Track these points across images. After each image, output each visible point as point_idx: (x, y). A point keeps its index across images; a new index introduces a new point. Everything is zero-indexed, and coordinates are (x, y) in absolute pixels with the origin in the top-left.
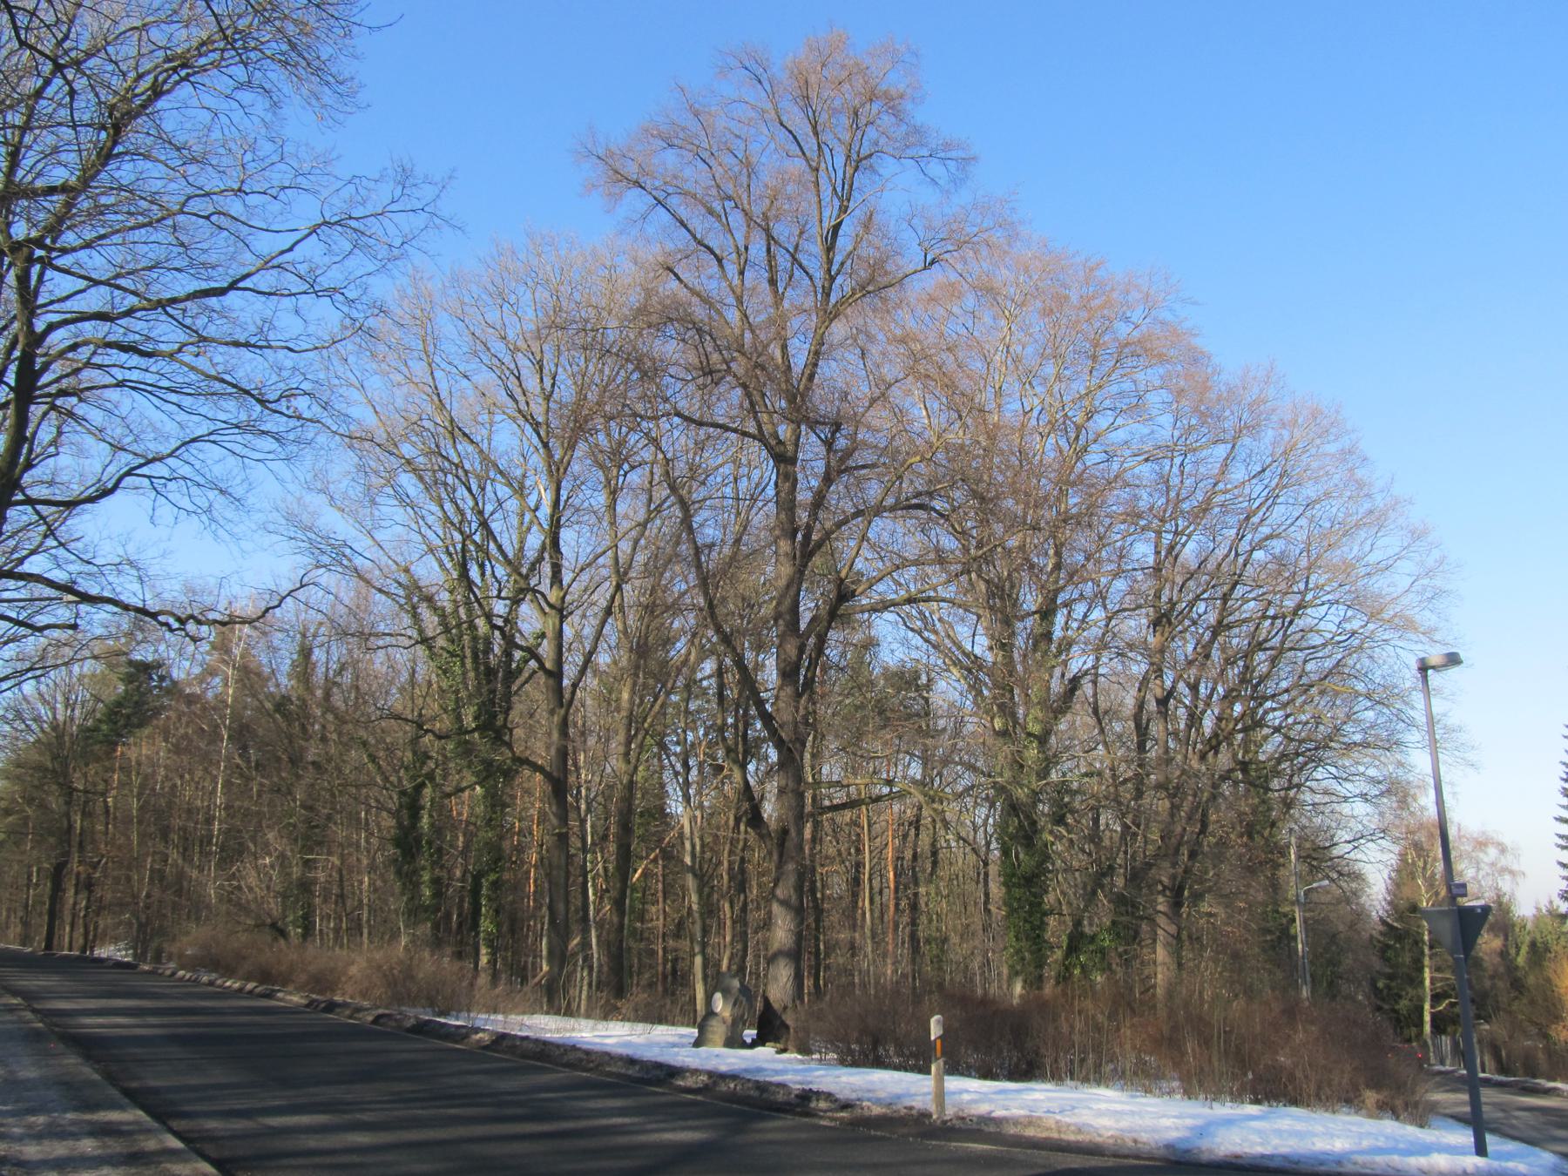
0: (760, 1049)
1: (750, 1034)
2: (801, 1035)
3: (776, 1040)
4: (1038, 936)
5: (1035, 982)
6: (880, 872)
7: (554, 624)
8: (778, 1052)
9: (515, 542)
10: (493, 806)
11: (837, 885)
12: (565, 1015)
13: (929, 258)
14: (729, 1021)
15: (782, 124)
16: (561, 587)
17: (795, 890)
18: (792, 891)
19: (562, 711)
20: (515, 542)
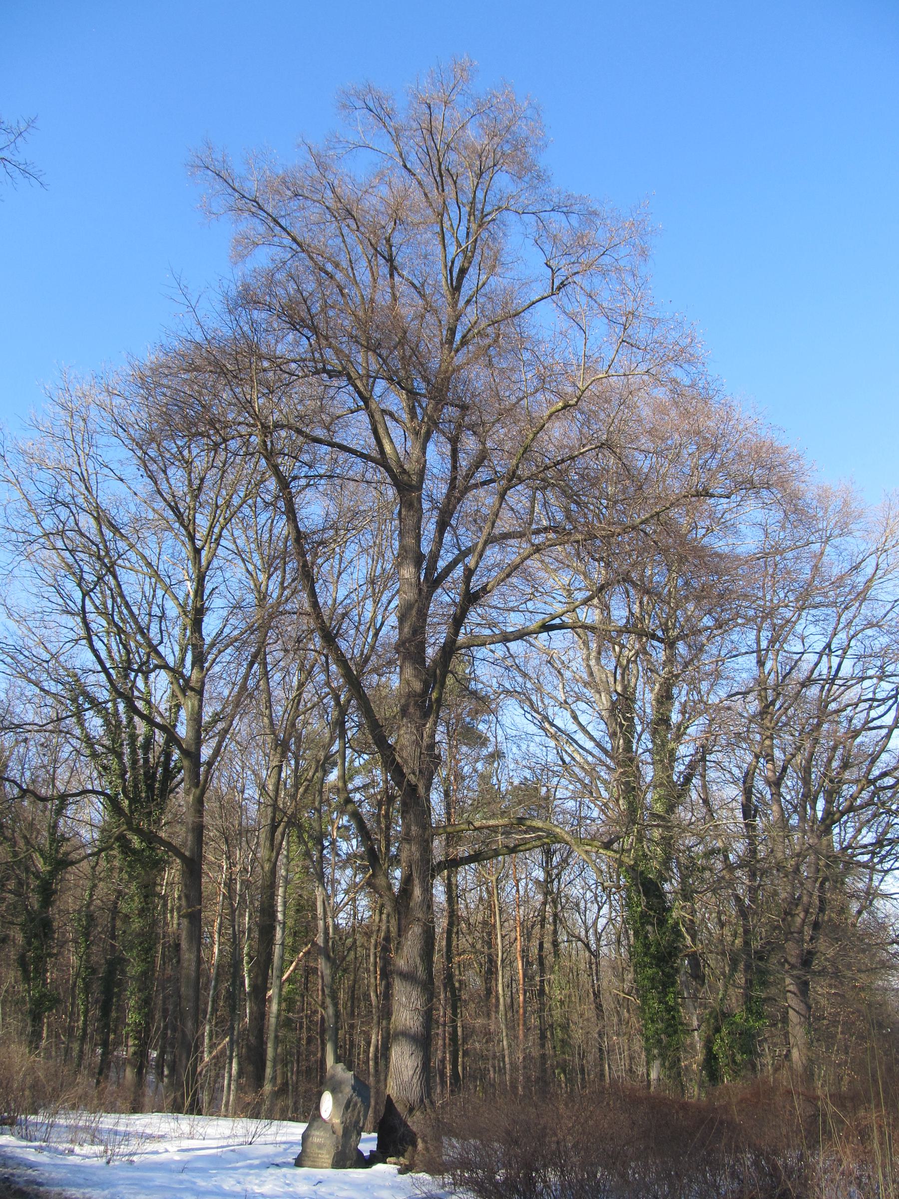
0: (379, 1167)
1: (368, 1143)
2: (493, 969)
3: (399, 1153)
4: (673, 1017)
5: (674, 1068)
6: (508, 963)
7: (193, 705)
8: (401, 1172)
9: (177, 654)
10: (146, 897)
11: (474, 980)
12: (191, 1111)
13: (556, 284)
14: (340, 1130)
15: (405, 166)
16: (202, 668)
17: (422, 960)
18: (418, 960)
19: (198, 792)
20: (177, 654)
